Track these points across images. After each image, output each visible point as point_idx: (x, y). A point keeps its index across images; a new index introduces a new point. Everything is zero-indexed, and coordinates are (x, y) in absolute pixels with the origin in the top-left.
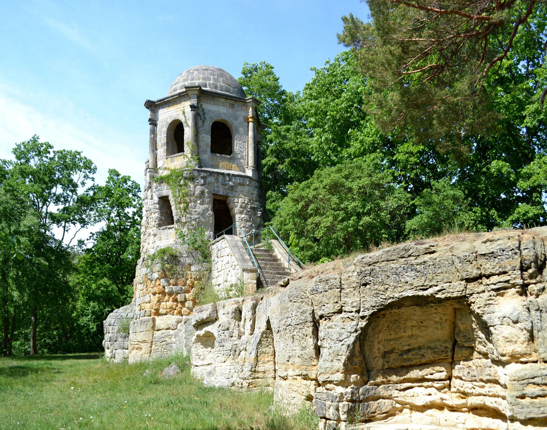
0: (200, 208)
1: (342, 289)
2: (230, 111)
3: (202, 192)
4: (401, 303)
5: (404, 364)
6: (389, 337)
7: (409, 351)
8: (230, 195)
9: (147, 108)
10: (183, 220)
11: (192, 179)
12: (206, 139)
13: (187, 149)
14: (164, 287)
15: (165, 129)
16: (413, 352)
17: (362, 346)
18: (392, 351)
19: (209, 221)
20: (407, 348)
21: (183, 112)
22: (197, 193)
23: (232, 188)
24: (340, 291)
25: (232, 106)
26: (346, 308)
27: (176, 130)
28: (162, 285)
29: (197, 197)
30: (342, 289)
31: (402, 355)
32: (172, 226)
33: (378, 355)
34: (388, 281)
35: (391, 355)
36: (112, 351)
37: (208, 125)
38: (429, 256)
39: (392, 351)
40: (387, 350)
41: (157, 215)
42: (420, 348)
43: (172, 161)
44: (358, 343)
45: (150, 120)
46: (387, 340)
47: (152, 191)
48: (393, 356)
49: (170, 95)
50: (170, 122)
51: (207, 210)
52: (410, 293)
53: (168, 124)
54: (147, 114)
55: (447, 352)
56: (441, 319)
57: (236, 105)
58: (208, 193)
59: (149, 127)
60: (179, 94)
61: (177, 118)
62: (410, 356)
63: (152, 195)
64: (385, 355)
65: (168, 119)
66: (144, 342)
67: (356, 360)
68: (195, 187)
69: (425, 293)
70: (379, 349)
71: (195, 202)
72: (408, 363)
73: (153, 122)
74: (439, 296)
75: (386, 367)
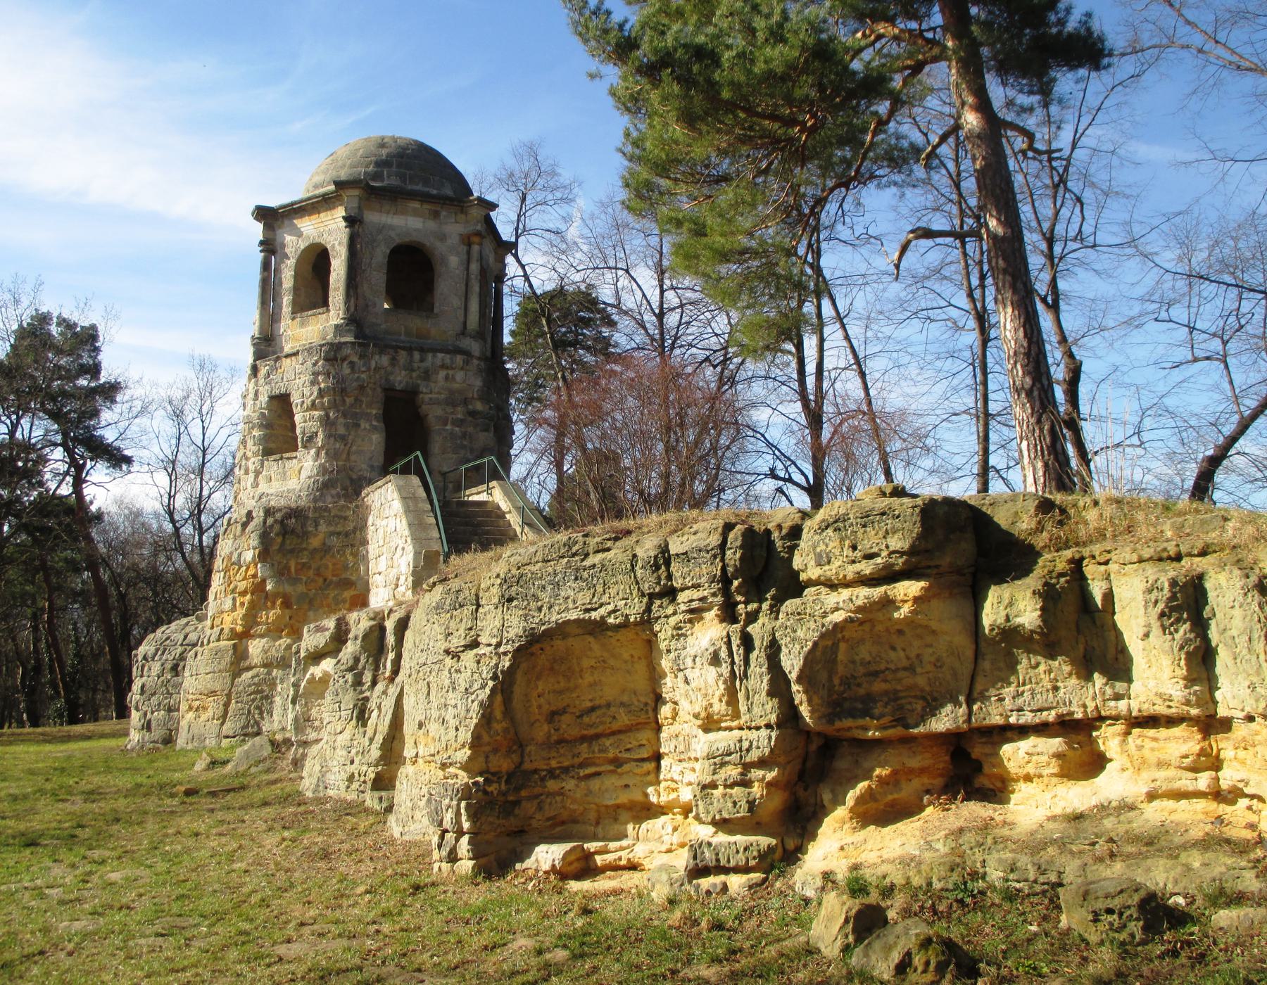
1: (478, 606)
2: (431, 225)
4: (562, 629)
5: (585, 732)
6: (557, 687)
7: (593, 709)
9: (256, 219)
12: (377, 278)
13: (337, 295)
16: (599, 712)
17: (507, 701)
18: (563, 711)
20: (589, 704)
21: (329, 228)
24: (477, 610)
25: (435, 215)
26: (483, 640)
27: (318, 259)
30: (478, 606)
31: (581, 716)
32: (294, 454)
33: (538, 717)
34: (541, 595)
35: (563, 718)
36: (145, 714)
37: (380, 254)
38: (600, 556)
39: (563, 711)
40: (554, 708)
42: (608, 705)
43: (303, 324)
44: (499, 698)
45: (262, 243)
46: (554, 691)
47: (256, 384)
48: (566, 718)
49: (307, 195)
52: (573, 615)
54: (258, 229)
55: (647, 712)
56: (632, 656)
57: (444, 213)
60: (324, 195)
61: (317, 240)
62: (594, 715)
63: (257, 392)
64: (553, 716)
66: (213, 693)
67: (498, 727)
69: (595, 615)
70: (540, 707)
72: (592, 731)
73: (270, 247)
74: (611, 620)
75: (555, 738)
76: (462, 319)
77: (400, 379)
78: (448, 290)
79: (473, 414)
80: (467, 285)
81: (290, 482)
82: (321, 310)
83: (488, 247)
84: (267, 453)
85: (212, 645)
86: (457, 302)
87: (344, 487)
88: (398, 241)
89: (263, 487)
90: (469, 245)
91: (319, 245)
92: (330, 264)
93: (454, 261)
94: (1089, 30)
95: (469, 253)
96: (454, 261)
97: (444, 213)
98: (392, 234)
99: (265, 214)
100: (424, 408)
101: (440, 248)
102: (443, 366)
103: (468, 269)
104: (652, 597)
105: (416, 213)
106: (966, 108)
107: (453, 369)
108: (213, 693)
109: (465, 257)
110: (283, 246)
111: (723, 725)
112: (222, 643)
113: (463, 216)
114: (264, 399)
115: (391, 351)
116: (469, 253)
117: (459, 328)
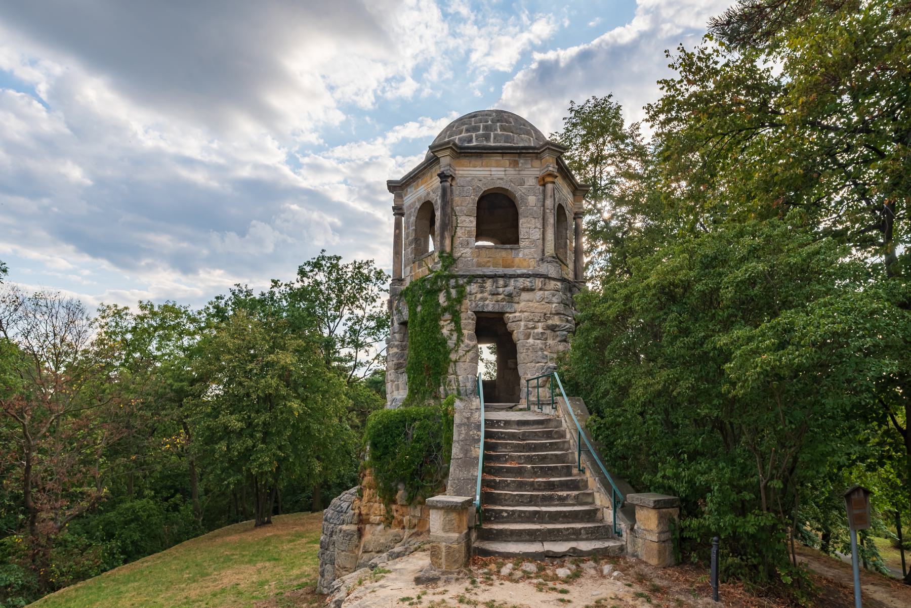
2: (511, 171)
25: (515, 164)
76: (541, 246)
77: (490, 306)
78: (529, 228)
79: (553, 328)
80: (543, 219)
83: (565, 192)
86: (537, 235)
87: (273, 435)
90: (544, 185)
93: (532, 200)
95: (544, 191)
96: (532, 200)
97: (522, 161)
99: (393, 186)
100: (511, 326)
101: (519, 191)
102: (525, 289)
103: (544, 206)
107: (533, 290)
109: (541, 197)
110: (277, 77)
111: (448, 249)
113: (539, 162)
115: (480, 280)
116: (544, 191)
117: (538, 257)
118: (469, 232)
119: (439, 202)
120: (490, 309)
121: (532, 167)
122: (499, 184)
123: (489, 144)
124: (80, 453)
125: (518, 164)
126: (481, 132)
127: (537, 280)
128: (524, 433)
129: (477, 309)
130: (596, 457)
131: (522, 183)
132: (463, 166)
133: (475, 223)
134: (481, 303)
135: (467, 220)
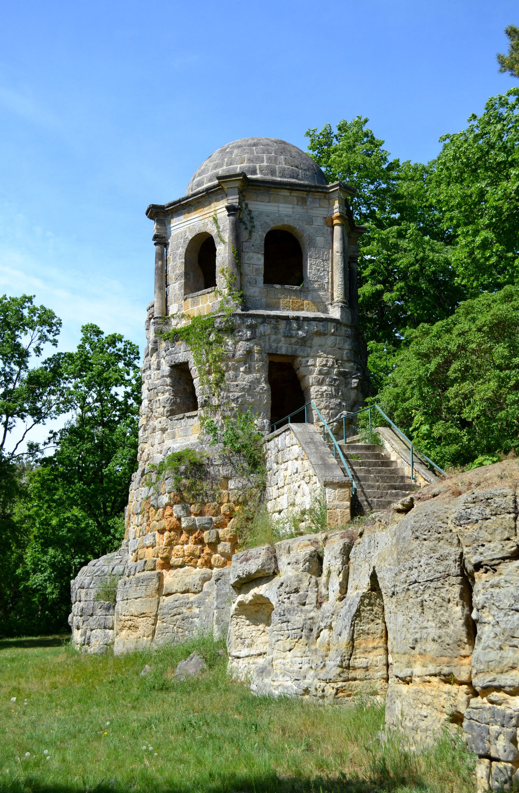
0: (245, 379)
2: (299, 209)
3: (249, 353)
8: (299, 353)
9: (151, 218)
10: (215, 401)
11: (231, 330)
12: (256, 261)
14: (179, 519)
15: (182, 251)
19: (261, 400)
21: (215, 219)
22: (240, 353)
23: (303, 342)
25: (303, 201)
28: (175, 515)
29: (238, 361)
32: (194, 413)
36: (85, 632)
37: (259, 237)
41: (167, 395)
43: (194, 304)
45: (155, 237)
50: (190, 238)
51: (258, 381)
53: (188, 242)
58: (260, 352)
59: (153, 249)
61: (203, 230)
65: (188, 234)
66: (143, 615)
68: (236, 343)
71: (236, 369)
73: (161, 241)
77: (284, 348)
81: (192, 438)
82: (209, 290)
84: (172, 413)
85: (137, 575)
88: (272, 225)
89: (168, 443)
91: (206, 233)
92: (215, 250)
94: (300, 774)
98: (268, 220)
102: (319, 334)
104: (469, 683)
105: (286, 201)
106: (169, 676)
107: (325, 334)
108: (143, 615)
112: (146, 573)
114: (166, 368)
118: (257, 270)
119: (227, 236)
120: (283, 351)
121: (320, 207)
122: (288, 221)
123: (274, 178)
124: (340, 677)
125: (306, 202)
126: (265, 164)
127: (329, 324)
128: (357, 454)
129: (270, 352)
130: (14, 640)
131: (310, 222)
132: (229, 249)
133: (262, 261)
134: (274, 345)
135: (255, 258)
